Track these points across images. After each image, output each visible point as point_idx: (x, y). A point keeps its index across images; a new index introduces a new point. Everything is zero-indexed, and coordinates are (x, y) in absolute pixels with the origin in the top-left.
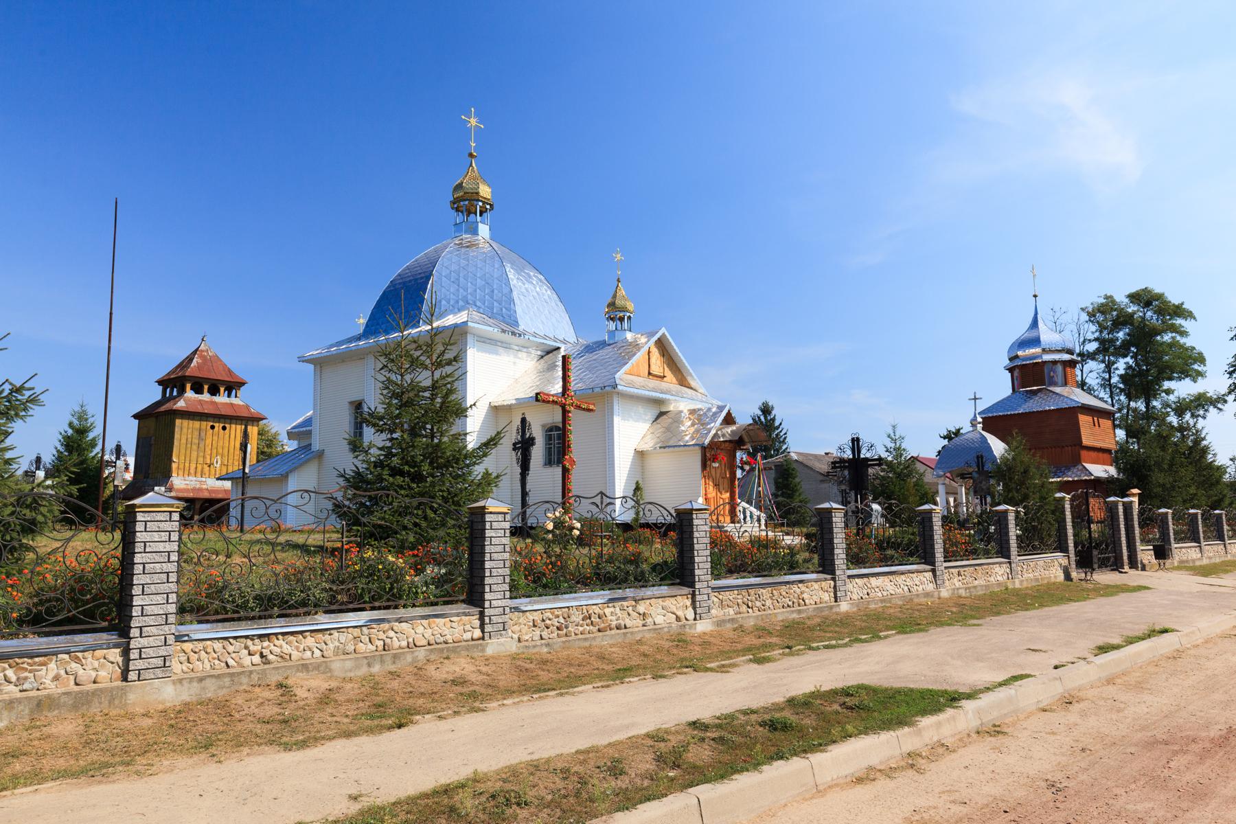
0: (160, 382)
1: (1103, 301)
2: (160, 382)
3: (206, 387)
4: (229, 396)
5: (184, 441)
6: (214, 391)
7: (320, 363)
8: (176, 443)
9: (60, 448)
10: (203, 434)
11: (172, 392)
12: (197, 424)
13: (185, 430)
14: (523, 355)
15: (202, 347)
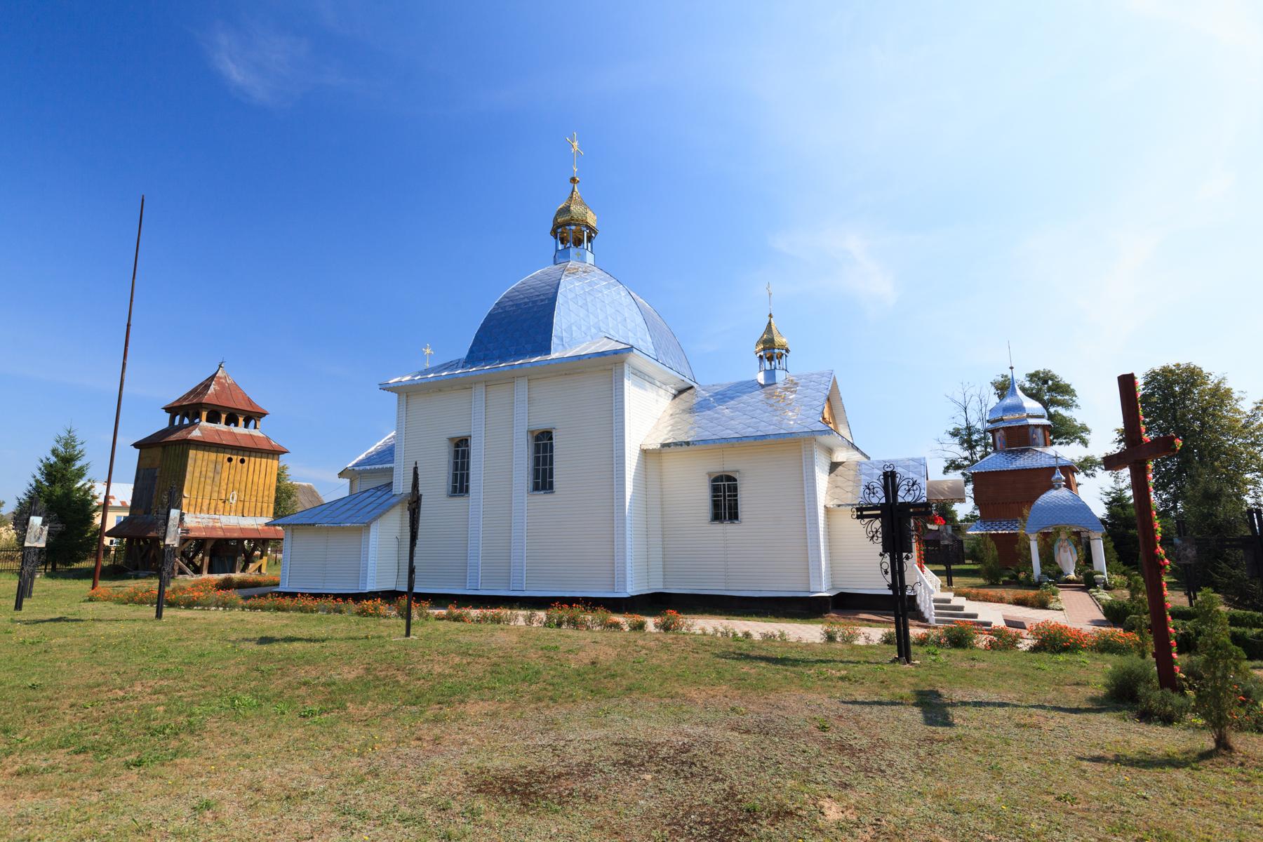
0: (167, 409)
1: (1001, 379)
2: (167, 409)
3: (224, 416)
4: (246, 426)
5: (197, 474)
6: (232, 420)
7: (404, 392)
8: (188, 476)
9: (39, 477)
10: (219, 467)
11: (182, 420)
12: (213, 456)
13: (199, 462)
14: (662, 392)
15: (220, 374)
